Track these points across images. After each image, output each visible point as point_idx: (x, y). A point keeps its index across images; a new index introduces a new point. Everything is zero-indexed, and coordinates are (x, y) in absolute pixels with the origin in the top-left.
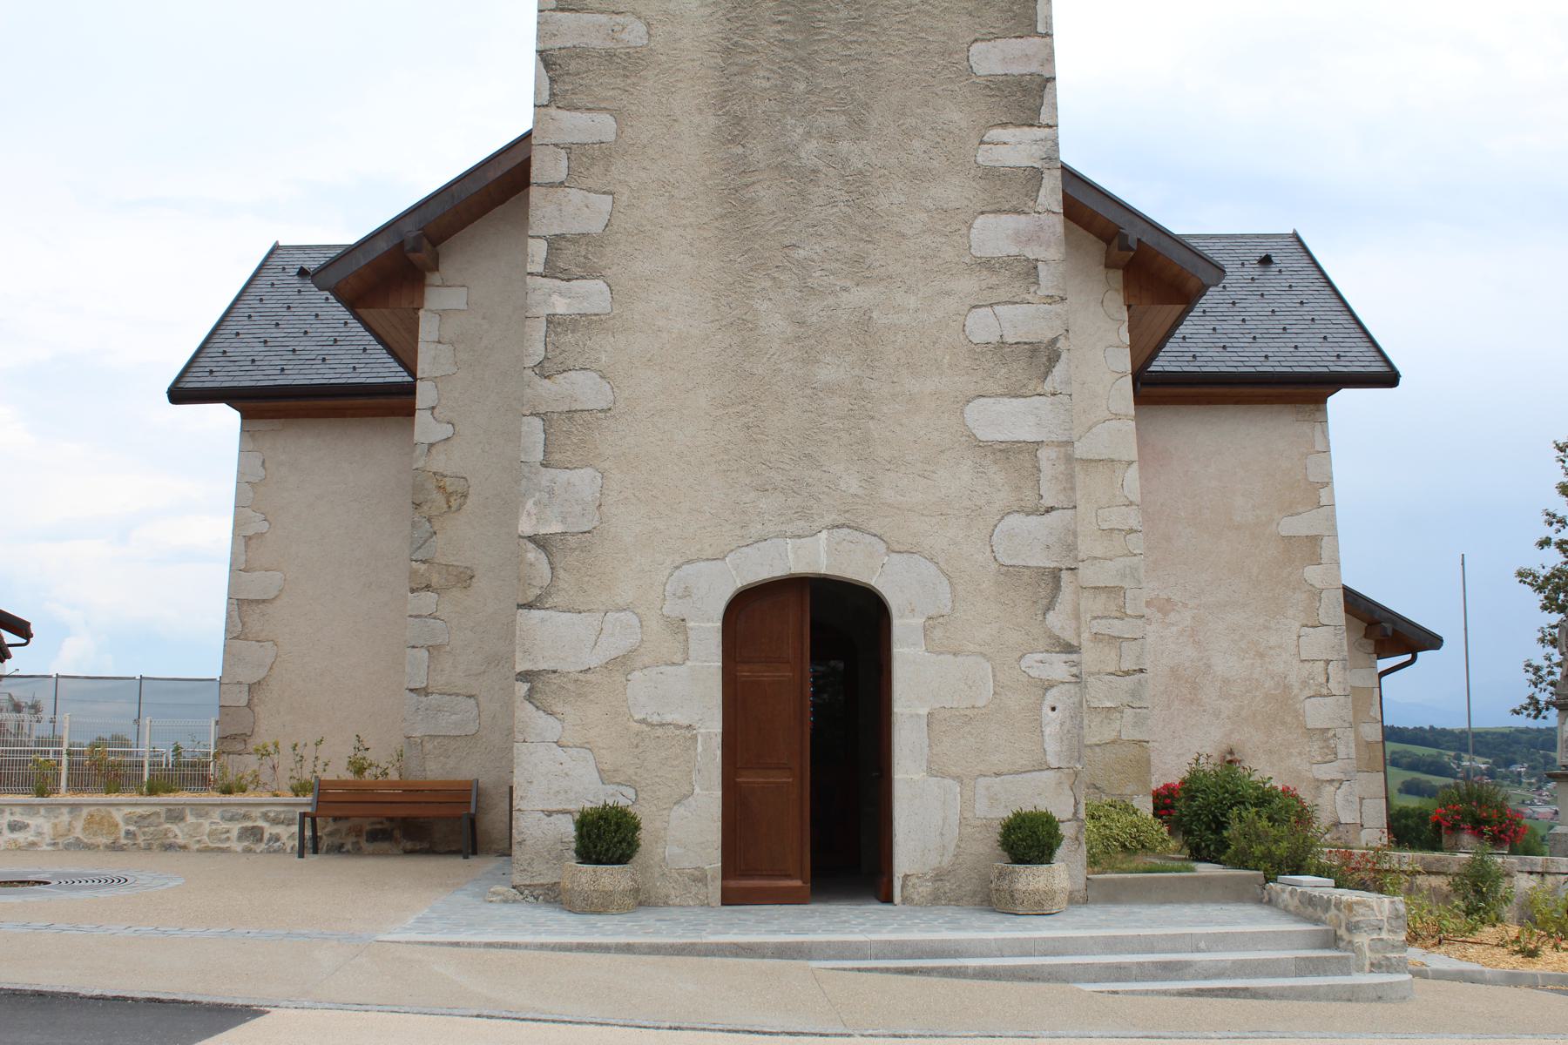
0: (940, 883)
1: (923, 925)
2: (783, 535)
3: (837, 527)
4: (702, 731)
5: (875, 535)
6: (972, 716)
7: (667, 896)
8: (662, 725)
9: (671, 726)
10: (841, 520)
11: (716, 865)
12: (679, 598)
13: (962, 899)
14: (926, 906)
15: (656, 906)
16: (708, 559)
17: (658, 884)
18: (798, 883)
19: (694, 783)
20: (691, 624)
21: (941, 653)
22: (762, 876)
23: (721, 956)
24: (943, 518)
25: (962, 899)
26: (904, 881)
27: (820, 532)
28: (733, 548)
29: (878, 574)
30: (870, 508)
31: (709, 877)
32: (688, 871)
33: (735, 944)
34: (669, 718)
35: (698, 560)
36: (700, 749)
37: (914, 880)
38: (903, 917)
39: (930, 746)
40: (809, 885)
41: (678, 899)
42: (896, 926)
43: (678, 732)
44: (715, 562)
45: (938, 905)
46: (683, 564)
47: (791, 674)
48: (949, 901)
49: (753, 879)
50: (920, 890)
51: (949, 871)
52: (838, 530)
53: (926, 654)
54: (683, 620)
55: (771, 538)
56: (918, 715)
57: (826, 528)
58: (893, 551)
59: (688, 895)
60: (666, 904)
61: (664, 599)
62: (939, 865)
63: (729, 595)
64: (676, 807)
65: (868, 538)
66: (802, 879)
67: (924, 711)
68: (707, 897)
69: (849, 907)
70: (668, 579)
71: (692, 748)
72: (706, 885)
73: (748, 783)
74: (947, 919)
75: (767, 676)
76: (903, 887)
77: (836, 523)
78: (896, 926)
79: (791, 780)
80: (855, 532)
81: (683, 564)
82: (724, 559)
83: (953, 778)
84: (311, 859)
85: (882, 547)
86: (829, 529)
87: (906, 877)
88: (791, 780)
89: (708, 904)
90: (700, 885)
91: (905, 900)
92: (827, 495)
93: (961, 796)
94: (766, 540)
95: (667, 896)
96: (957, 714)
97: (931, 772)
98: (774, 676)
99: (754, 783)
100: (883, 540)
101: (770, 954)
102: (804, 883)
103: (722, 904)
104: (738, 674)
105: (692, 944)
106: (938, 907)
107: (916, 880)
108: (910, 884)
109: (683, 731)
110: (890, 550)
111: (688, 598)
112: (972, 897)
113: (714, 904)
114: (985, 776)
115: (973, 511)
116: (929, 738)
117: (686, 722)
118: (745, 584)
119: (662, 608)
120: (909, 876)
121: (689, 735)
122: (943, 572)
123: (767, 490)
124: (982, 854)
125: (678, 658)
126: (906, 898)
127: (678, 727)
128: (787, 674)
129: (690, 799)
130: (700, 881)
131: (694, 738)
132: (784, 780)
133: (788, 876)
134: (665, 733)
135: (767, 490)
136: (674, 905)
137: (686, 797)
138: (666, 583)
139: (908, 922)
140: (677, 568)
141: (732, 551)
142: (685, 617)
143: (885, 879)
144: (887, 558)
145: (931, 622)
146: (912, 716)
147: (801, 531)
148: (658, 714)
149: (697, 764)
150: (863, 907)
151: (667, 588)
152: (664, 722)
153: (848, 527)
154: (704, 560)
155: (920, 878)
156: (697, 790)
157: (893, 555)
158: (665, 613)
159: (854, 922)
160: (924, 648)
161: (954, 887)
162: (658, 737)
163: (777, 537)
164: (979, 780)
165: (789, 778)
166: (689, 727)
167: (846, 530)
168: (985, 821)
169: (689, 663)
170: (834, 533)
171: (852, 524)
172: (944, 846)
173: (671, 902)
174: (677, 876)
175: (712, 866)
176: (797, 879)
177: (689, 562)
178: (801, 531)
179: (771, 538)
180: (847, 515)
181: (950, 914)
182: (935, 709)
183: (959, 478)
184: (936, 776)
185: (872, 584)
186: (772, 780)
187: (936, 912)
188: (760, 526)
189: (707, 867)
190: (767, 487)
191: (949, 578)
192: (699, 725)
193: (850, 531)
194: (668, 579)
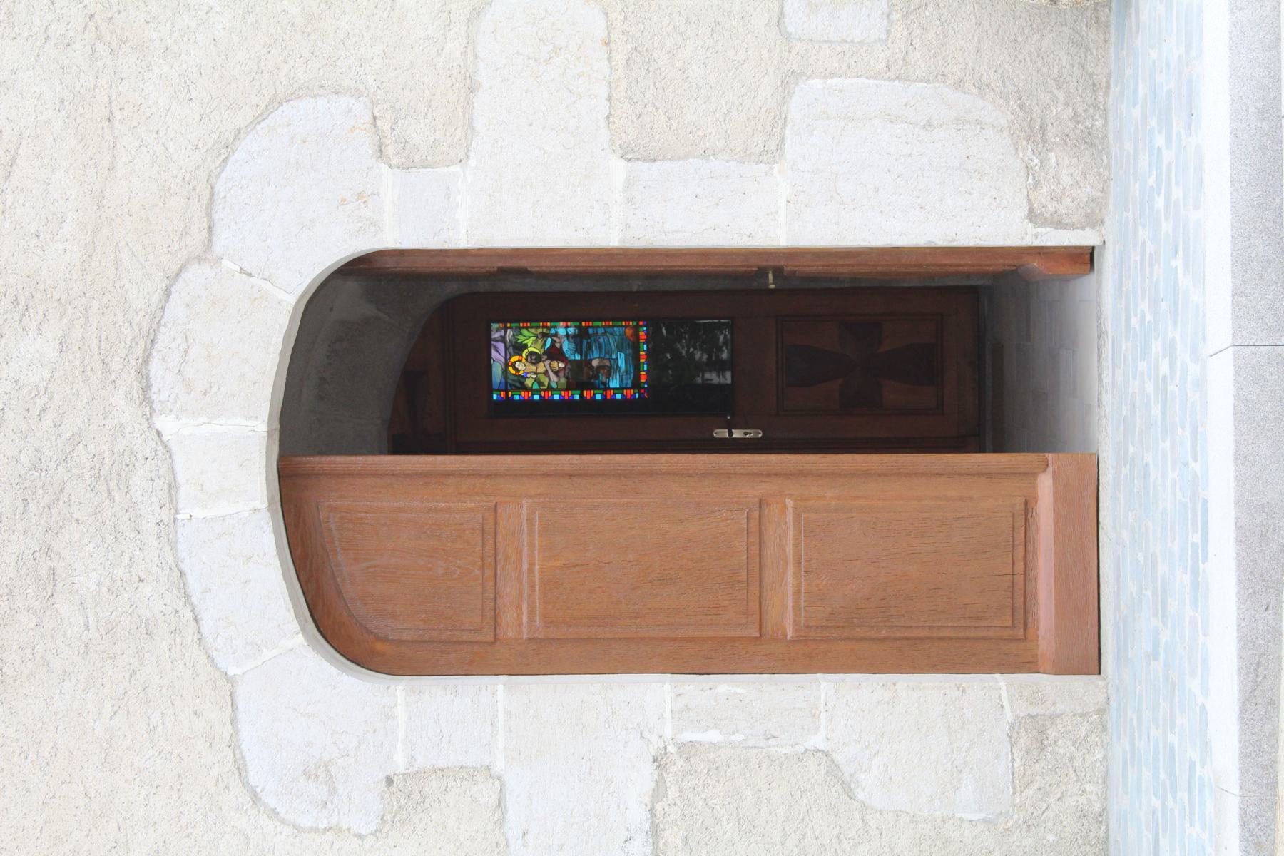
0: (1051, 132)
1: (1177, 193)
2: (169, 529)
3: (146, 389)
4: (668, 732)
5: (167, 293)
6: (629, 46)
7: (1082, 815)
8: (655, 831)
9: (659, 806)
10: (129, 379)
11: (1004, 693)
12: (333, 791)
13: (1091, 75)
14: (1108, 167)
15: (1106, 840)
16: (233, 722)
17: (1051, 838)
18: (1045, 485)
19: (800, 749)
20: (400, 763)
21: (470, 124)
22: (1027, 573)
23: (1275, 747)
24: (118, 115)
25: (1091, 75)
26: (1045, 222)
27: (159, 434)
28: (204, 658)
29: (267, 285)
30: (95, 305)
31: (1033, 711)
32: (1018, 763)
33: (1243, 709)
34: (638, 815)
35: (234, 744)
36: (713, 736)
37: (1042, 197)
38: (1144, 234)
39: (705, 154)
40: (1050, 456)
41: (1088, 787)
42: (1178, 263)
43: (673, 792)
44: (240, 704)
45: (1105, 137)
46: (245, 783)
47: (524, 502)
48: (1095, 107)
49: (1035, 593)
50: (1066, 180)
51: (1021, 107)
52: (154, 389)
53: (472, 162)
54: (390, 781)
55: (176, 559)
56: (628, 186)
57: (149, 418)
58: (209, 245)
59: (1078, 762)
60: (1101, 817)
61: (337, 830)
62: (1005, 133)
63: (325, 664)
64: (860, 795)
65: (176, 309)
66: (1032, 475)
67: (618, 170)
68: (1083, 715)
69: (1107, 362)
70: (283, 822)
71: (712, 756)
72: (1053, 718)
73: (797, 608)
74: (1153, 123)
75: (532, 565)
76: (1059, 224)
77: (136, 393)
78: (1178, 263)
79: (789, 503)
80: (159, 344)
81: (245, 783)
82: (231, 680)
83: (787, 95)
84: (621, 159)
85: (197, 275)
86: (152, 410)
87: (1033, 216)
88: (789, 503)
89: (1101, 712)
90: (1052, 733)
91: (1093, 220)
92: (62, 415)
93: (832, 75)
94: (182, 574)
95: (1082, 815)
96: (623, 84)
97: (772, 153)
98: (531, 545)
99: (797, 593)
100: (178, 275)
101: (1269, 615)
102: (1045, 470)
103: (1092, 663)
104: (525, 637)
105: (1244, 824)
106: (1111, 136)
107: (1045, 190)
108: (1051, 207)
109: (670, 779)
110: (206, 254)
111: (333, 770)
112: (1087, 49)
113: (1101, 698)
114: (781, 14)
115: (99, 38)
116: (686, 157)
117: (649, 770)
118: (295, 626)
119: (360, 836)
120: (1031, 210)
121: (680, 762)
122: (259, 119)
123: (52, 571)
124: (979, 24)
125: (486, 793)
126: (1086, 216)
127: (659, 791)
128: (525, 512)
129: (838, 757)
130: (1042, 731)
131: (687, 750)
132: (790, 518)
133: (1028, 508)
134: (674, 822)
135: (52, 571)
136: (1104, 798)
137: (834, 769)
138: (295, 827)
139: (1166, 227)
140: (255, 798)
141: (210, 658)
142: (382, 775)
143: (1035, 264)
144: (225, 262)
145: (390, 150)
146: (630, 201)
147: (159, 483)
148: (628, 840)
149: (752, 742)
150: (1109, 325)
151: (307, 822)
152: (647, 826)
153: (146, 362)
154: (236, 731)
155: (1036, 183)
156: (817, 741)
157: (218, 248)
158: (373, 827)
159: (1164, 368)
160: (456, 169)
161: (1060, 95)
162: (686, 840)
163: (173, 546)
164: (790, 29)
165: (785, 507)
166: (659, 762)
167: (155, 368)
168: (895, 16)
169: (499, 766)
170: (163, 397)
171: (139, 352)
172: (957, 120)
173: (1097, 807)
174: (1030, 791)
175: (1005, 702)
176: (1034, 487)
177: (241, 770)
178: (159, 483)
179: (176, 559)
180: (115, 365)
181: (1136, 112)
182: (613, 142)
183: (14, 72)
184: (782, 140)
185: (292, 299)
186: (789, 550)
187: (1129, 146)
188: (146, 589)
189: (1009, 716)
190: (44, 571)
191: (276, 102)
192: (655, 739)
193: (156, 358)
194: (283, 822)
